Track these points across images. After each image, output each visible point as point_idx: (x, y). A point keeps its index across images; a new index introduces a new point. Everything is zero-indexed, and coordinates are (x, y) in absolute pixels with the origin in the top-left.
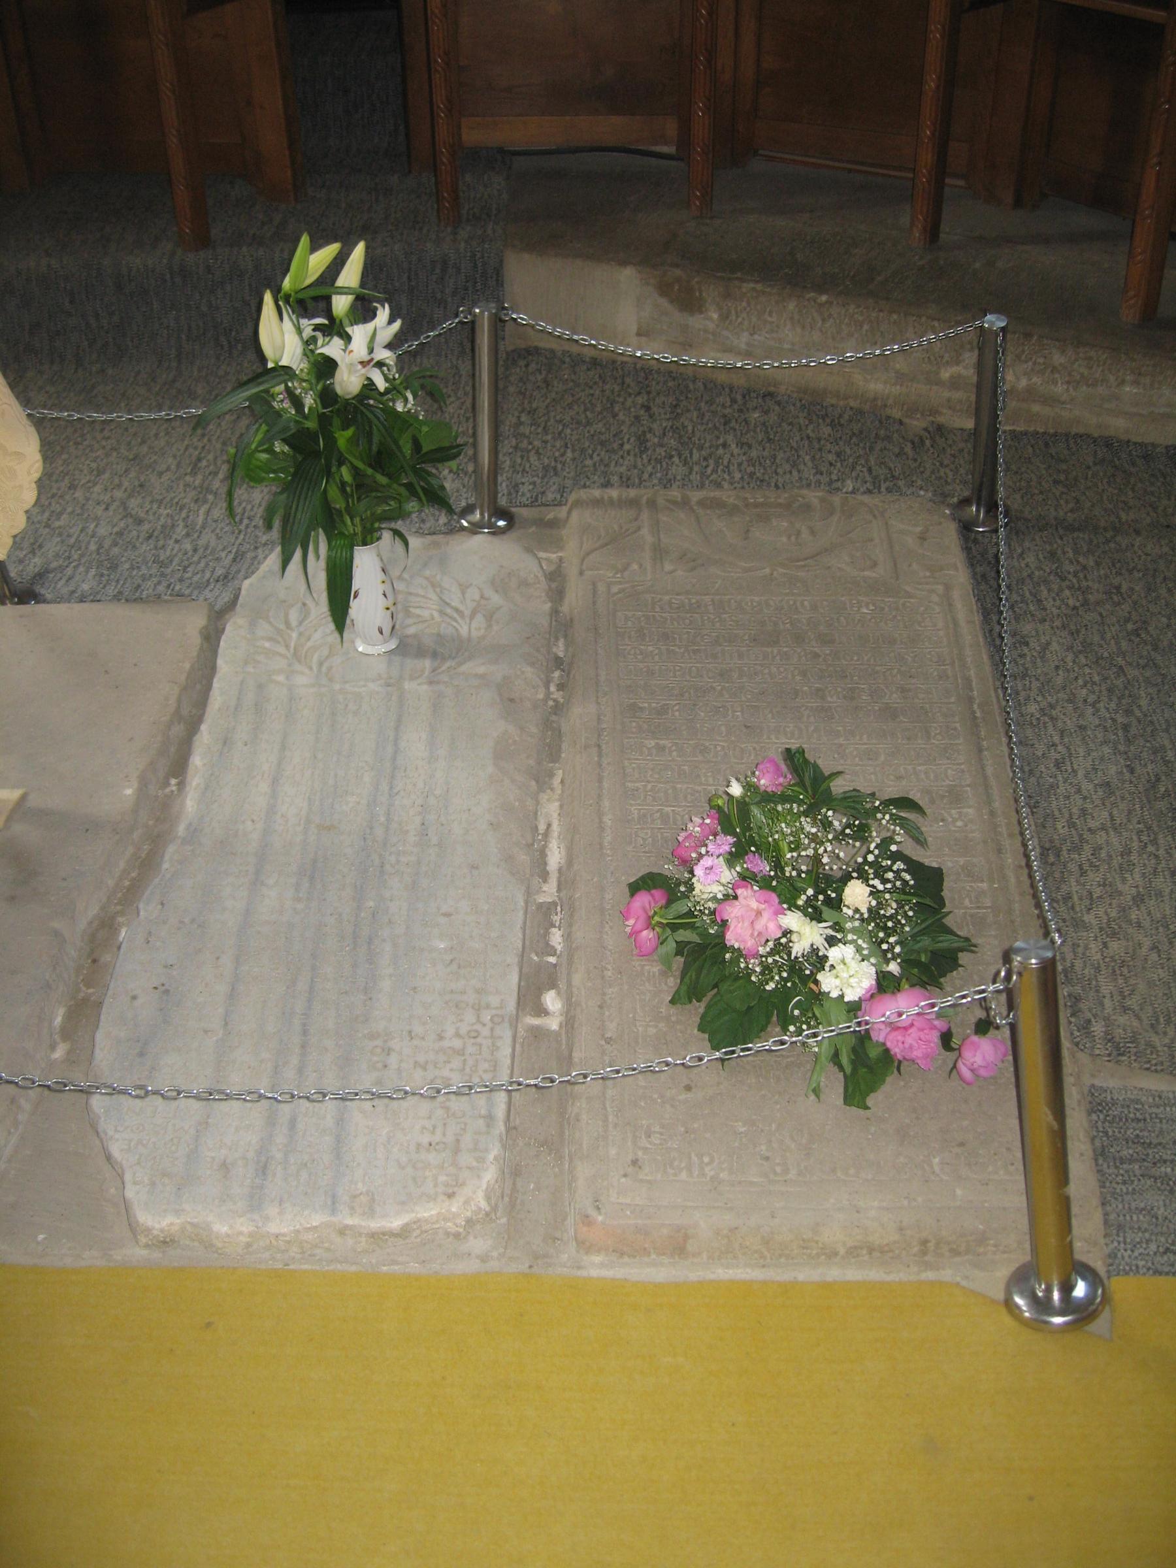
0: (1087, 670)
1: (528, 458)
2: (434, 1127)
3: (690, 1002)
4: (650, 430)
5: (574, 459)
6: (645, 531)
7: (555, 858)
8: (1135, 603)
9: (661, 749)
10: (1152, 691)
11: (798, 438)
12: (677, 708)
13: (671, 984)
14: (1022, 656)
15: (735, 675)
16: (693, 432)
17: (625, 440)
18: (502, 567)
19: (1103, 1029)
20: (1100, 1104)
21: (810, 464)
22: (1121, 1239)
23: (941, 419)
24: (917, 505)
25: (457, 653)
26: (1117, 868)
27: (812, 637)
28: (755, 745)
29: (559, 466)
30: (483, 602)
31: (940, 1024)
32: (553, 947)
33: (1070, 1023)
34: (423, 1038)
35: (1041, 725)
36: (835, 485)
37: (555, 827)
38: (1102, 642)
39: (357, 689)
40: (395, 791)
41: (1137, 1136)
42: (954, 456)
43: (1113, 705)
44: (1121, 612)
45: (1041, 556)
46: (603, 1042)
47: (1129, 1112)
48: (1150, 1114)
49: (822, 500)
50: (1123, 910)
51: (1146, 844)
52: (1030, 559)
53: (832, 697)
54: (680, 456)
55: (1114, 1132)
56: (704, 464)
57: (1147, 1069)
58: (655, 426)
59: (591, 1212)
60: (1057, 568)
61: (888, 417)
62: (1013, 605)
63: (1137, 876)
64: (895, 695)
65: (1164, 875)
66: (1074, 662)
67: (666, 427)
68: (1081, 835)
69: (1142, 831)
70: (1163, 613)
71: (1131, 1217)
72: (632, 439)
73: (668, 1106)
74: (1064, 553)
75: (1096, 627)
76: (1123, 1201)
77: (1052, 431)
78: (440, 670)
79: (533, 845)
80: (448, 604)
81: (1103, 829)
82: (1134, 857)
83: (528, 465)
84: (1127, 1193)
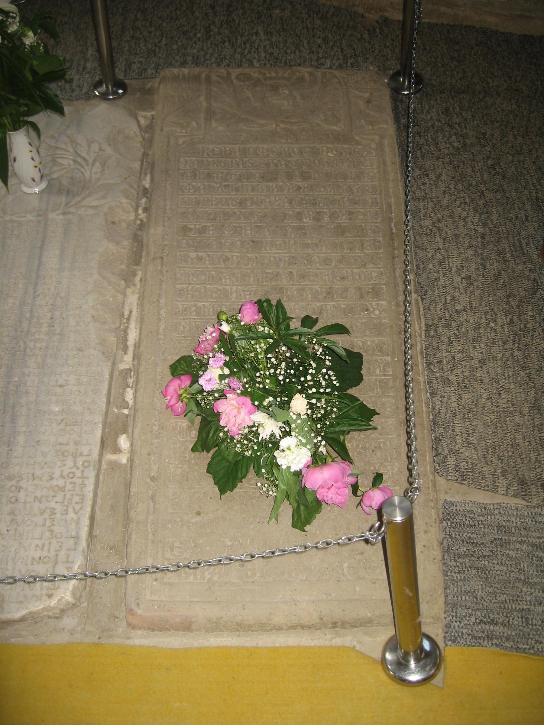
0: (462, 194)
1: (139, 43)
2: (43, 545)
3: (203, 451)
4: (214, 23)
5: (166, 45)
6: (202, 99)
7: (133, 336)
8: (494, 145)
9: (200, 259)
10: (499, 209)
11: (301, 28)
12: (211, 228)
13: (193, 436)
14: (424, 184)
15: (249, 203)
16: (239, 24)
17: (198, 31)
18: (114, 126)
19: (454, 463)
20: (449, 514)
21: (306, 46)
22: (454, 614)
23: (387, 14)
24: (368, 76)
25: (82, 191)
26: (471, 339)
27: (298, 174)
28: (257, 255)
29: (157, 50)
30: (101, 153)
31: (352, 480)
32: (127, 402)
33: (434, 461)
34: (41, 479)
35: (432, 234)
36: (320, 61)
37: (134, 313)
38: (473, 174)
39: (20, 219)
40: (37, 294)
41: (470, 537)
42: (393, 40)
43: (476, 220)
44: (485, 152)
45: (440, 112)
46: (149, 480)
47: (466, 520)
48: (478, 521)
49: (311, 74)
50: (473, 370)
51: (489, 321)
52: (434, 114)
53: (306, 218)
54: (230, 41)
55: (456, 535)
56: (243, 47)
57: (480, 489)
58: (216, 20)
59: (134, 606)
60: (449, 120)
61: (356, 13)
62: (421, 147)
63: (483, 345)
64: (344, 217)
65: (499, 344)
66: (455, 188)
67: (223, 21)
68: (451, 315)
69: (488, 312)
70: (510, 152)
71: (461, 597)
72: (202, 29)
73: (185, 527)
74: (454, 109)
75: (469, 162)
76: (457, 585)
77: (452, 23)
78: (70, 205)
79: (120, 327)
80: (79, 155)
81: (464, 310)
82: (482, 331)
83: (138, 50)
84: (460, 580)
